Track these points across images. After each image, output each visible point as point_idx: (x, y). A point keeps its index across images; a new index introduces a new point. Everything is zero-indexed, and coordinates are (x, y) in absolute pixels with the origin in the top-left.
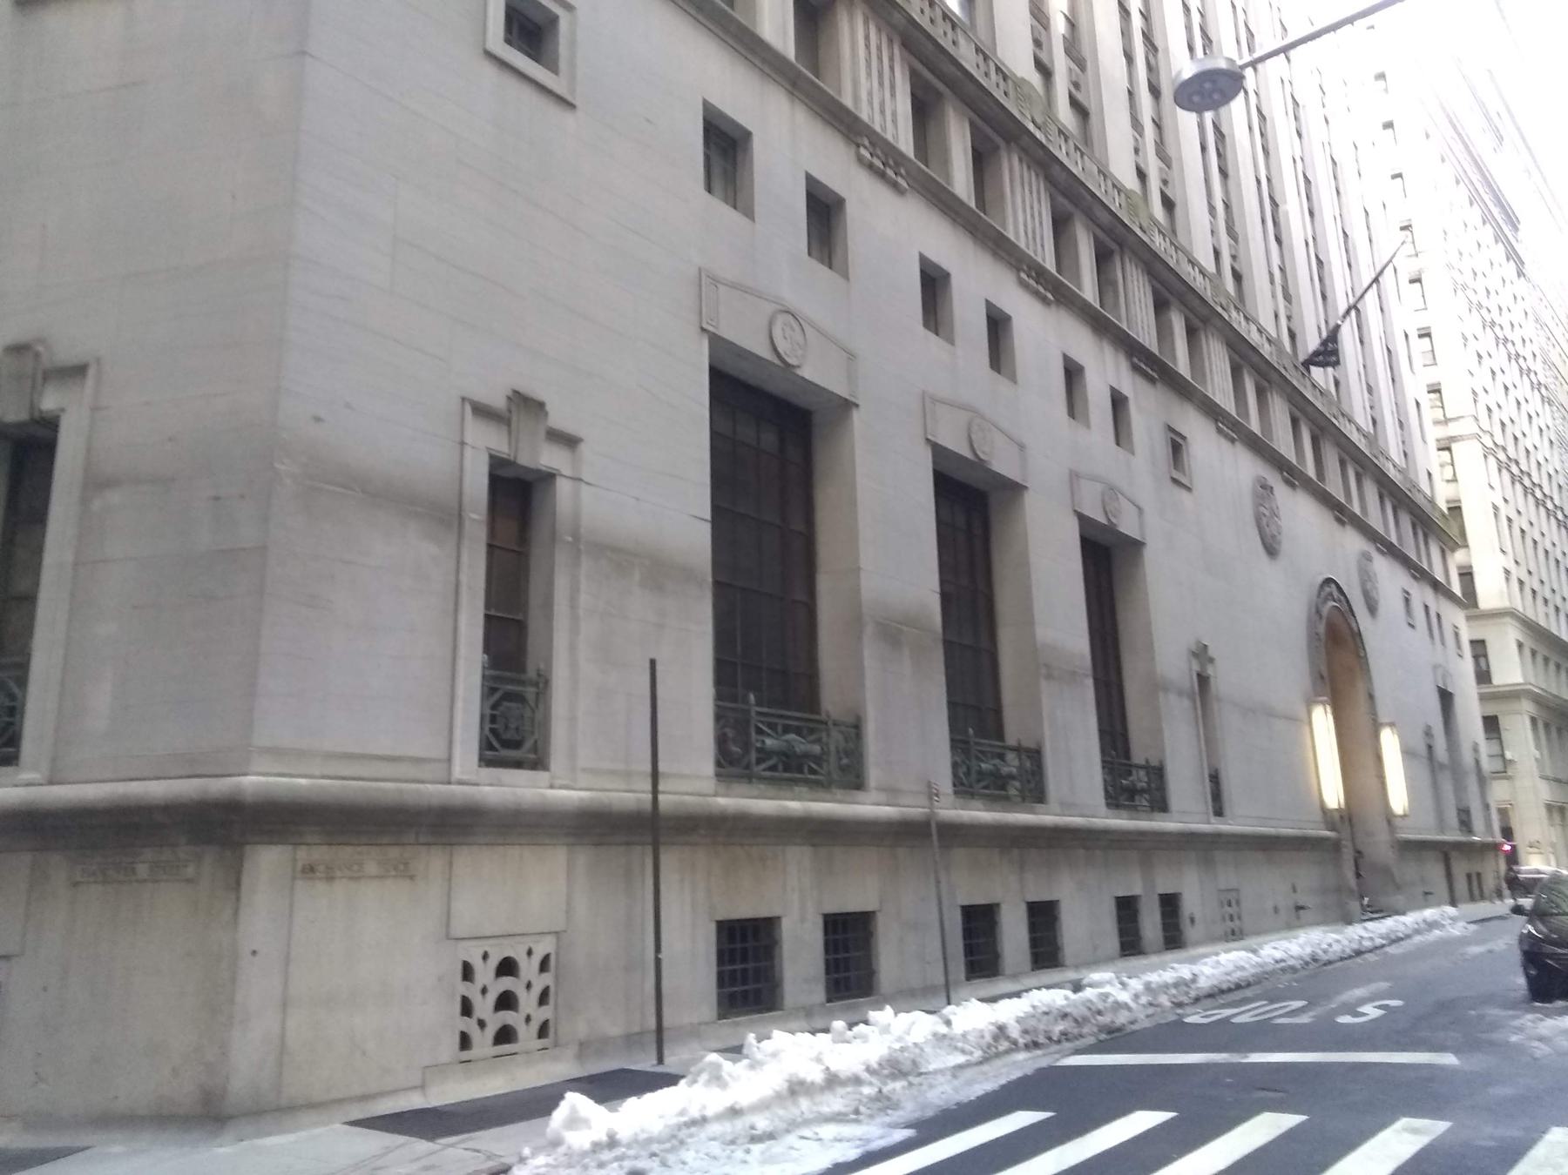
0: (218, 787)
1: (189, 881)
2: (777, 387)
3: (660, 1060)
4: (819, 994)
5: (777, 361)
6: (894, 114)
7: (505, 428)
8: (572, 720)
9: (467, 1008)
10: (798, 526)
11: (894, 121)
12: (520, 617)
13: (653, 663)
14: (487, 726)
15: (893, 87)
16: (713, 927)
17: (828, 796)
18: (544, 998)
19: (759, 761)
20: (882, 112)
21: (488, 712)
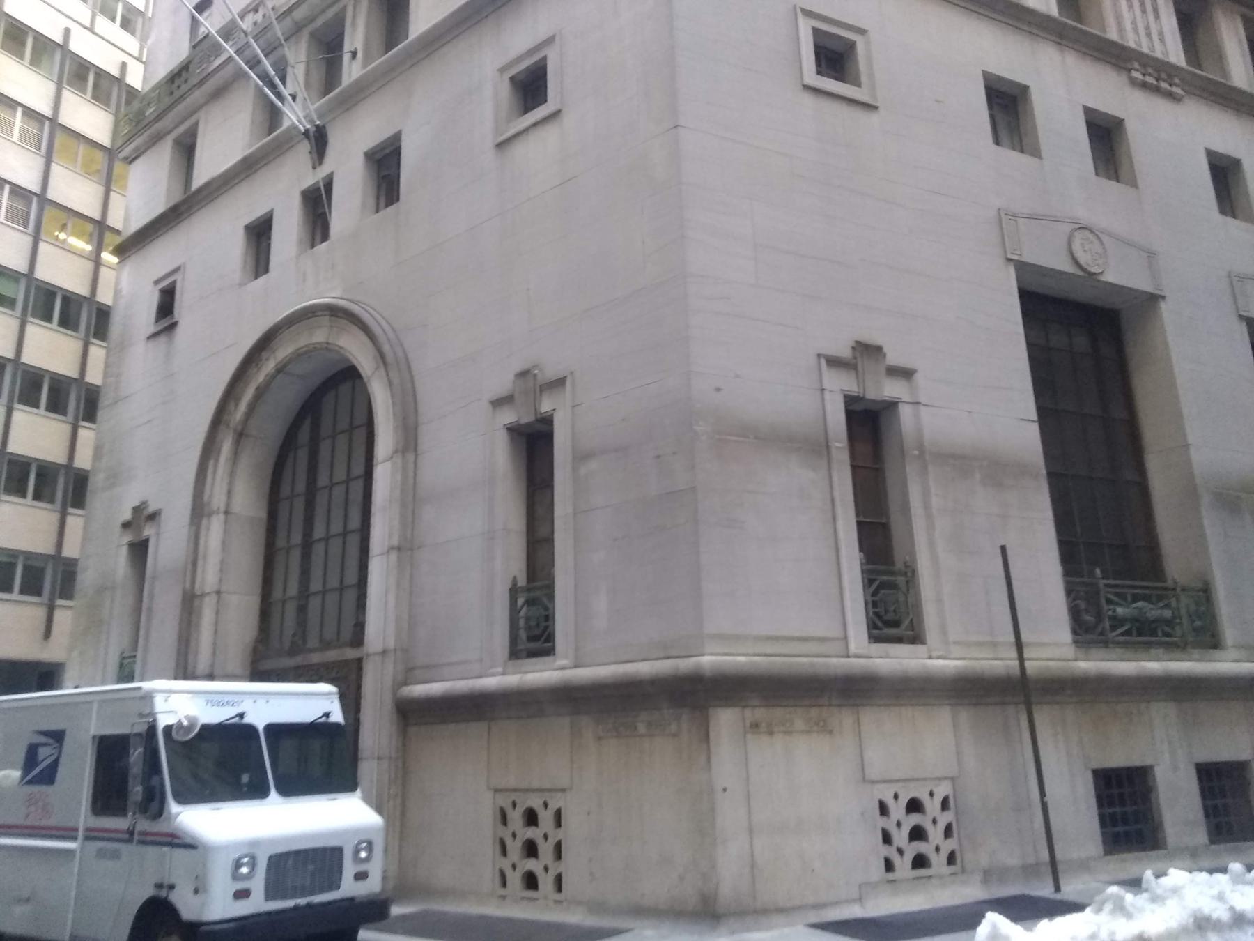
0: (685, 665)
1: (675, 735)
2: (1084, 294)
3: (1058, 889)
4: (1201, 837)
5: (1081, 273)
6: (1161, 34)
8: (939, 601)
9: (887, 838)
11: (1162, 40)
15: (1156, 10)
18: (948, 832)
19: (1113, 628)
20: (1149, 35)
21: (870, 599)
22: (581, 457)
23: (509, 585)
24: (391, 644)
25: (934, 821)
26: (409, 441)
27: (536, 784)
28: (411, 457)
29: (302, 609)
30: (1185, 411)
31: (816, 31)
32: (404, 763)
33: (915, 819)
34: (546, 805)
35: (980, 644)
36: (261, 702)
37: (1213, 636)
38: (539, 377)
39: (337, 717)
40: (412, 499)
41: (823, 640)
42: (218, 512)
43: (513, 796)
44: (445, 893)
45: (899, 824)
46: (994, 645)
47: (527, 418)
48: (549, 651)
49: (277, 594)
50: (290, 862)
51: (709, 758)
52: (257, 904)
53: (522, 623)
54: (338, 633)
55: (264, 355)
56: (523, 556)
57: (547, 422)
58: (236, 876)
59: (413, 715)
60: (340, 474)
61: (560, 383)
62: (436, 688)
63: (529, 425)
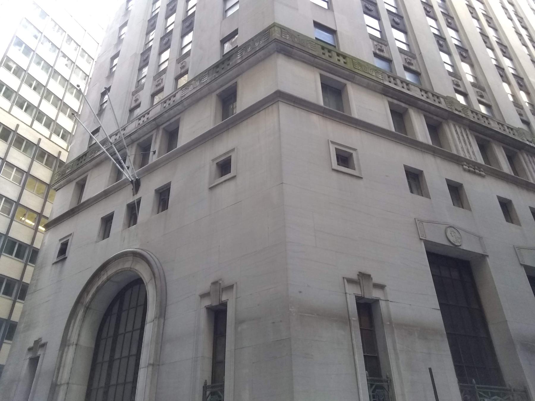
5: (451, 245)
13: (430, 369)
21: (371, 394)
22: (239, 322)
23: (203, 385)
26: (162, 314)
28: (162, 321)
31: (336, 149)
40: (161, 341)
49: (95, 385)
60: (129, 328)
61: (231, 287)
63: (216, 306)
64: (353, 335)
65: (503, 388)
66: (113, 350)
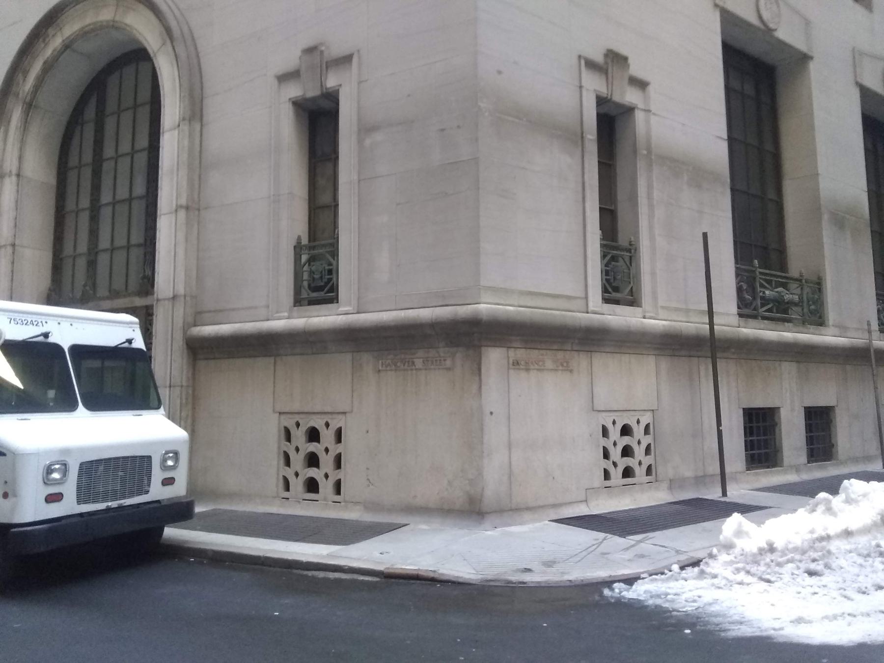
0: (464, 311)
1: (449, 369)
3: (724, 494)
4: (803, 459)
5: (762, 27)
7: (604, 77)
8: (653, 274)
9: (606, 455)
10: (769, 146)
12: (613, 208)
13: (705, 235)
14: (604, 277)
16: (741, 412)
17: (806, 330)
18: (648, 450)
19: (763, 305)
22: (366, 129)
23: (294, 243)
24: (181, 290)
25: (639, 442)
26: (195, 112)
27: (318, 408)
28: (197, 127)
29: (92, 264)
30: (818, 150)
32: (194, 391)
33: (626, 440)
34: (327, 425)
35: (677, 310)
36: (65, 324)
37: (820, 317)
38: (326, 54)
39: (139, 343)
40: (198, 164)
41: (569, 298)
42: (10, 175)
43: (297, 418)
44: (231, 496)
45: (615, 444)
46: (687, 311)
47: (313, 92)
48: (334, 300)
49: (68, 249)
50: (101, 468)
51: (480, 387)
52: (69, 506)
53: (306, 276)
54: (127, 286)
55: (51, 31)
56: (306, 219)
57: (332, 97)
58: (47, 482)
59: (201, 351)
60: (125, 147)
61: (347, 59)
62: (225, 329)
63: (314, 99)
64: (586, 165)
65: (784, 274)
66: (96, 188)
